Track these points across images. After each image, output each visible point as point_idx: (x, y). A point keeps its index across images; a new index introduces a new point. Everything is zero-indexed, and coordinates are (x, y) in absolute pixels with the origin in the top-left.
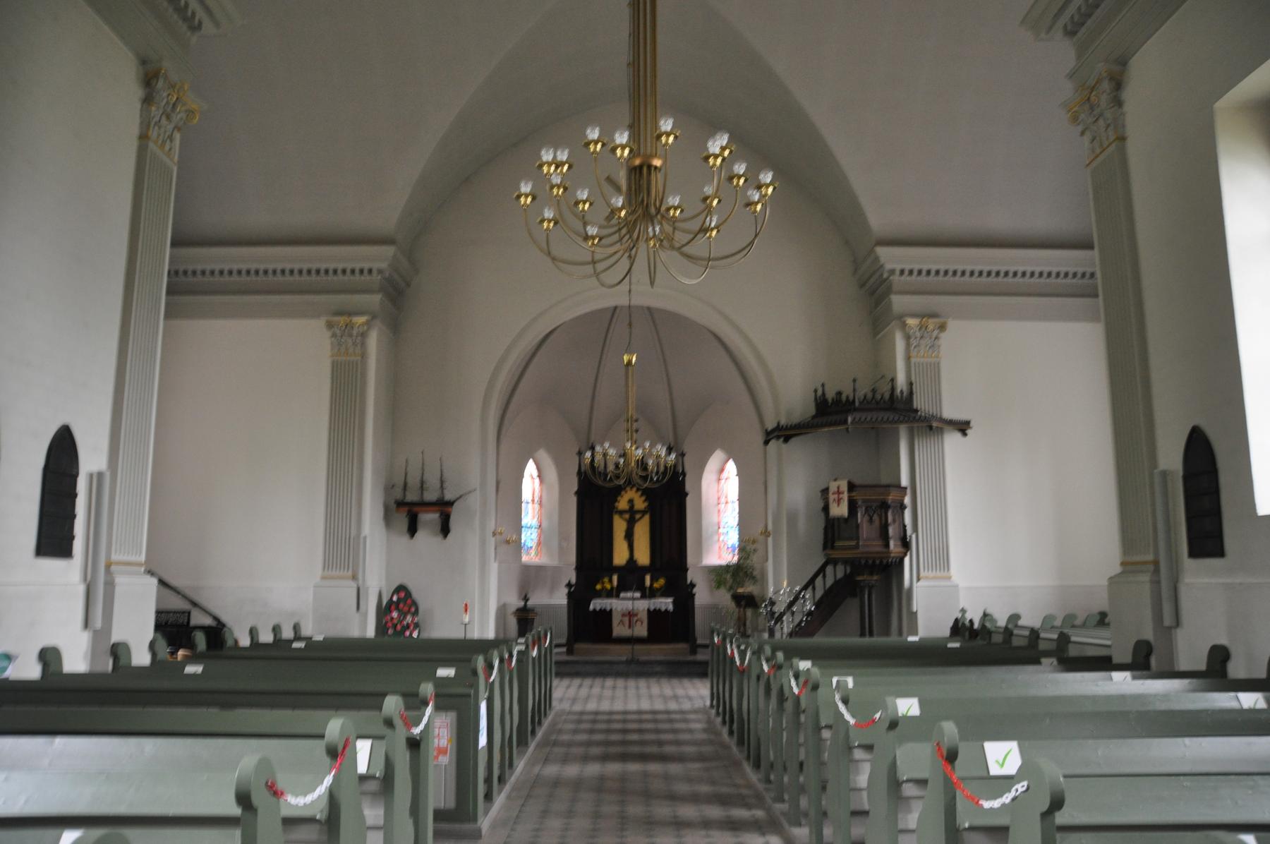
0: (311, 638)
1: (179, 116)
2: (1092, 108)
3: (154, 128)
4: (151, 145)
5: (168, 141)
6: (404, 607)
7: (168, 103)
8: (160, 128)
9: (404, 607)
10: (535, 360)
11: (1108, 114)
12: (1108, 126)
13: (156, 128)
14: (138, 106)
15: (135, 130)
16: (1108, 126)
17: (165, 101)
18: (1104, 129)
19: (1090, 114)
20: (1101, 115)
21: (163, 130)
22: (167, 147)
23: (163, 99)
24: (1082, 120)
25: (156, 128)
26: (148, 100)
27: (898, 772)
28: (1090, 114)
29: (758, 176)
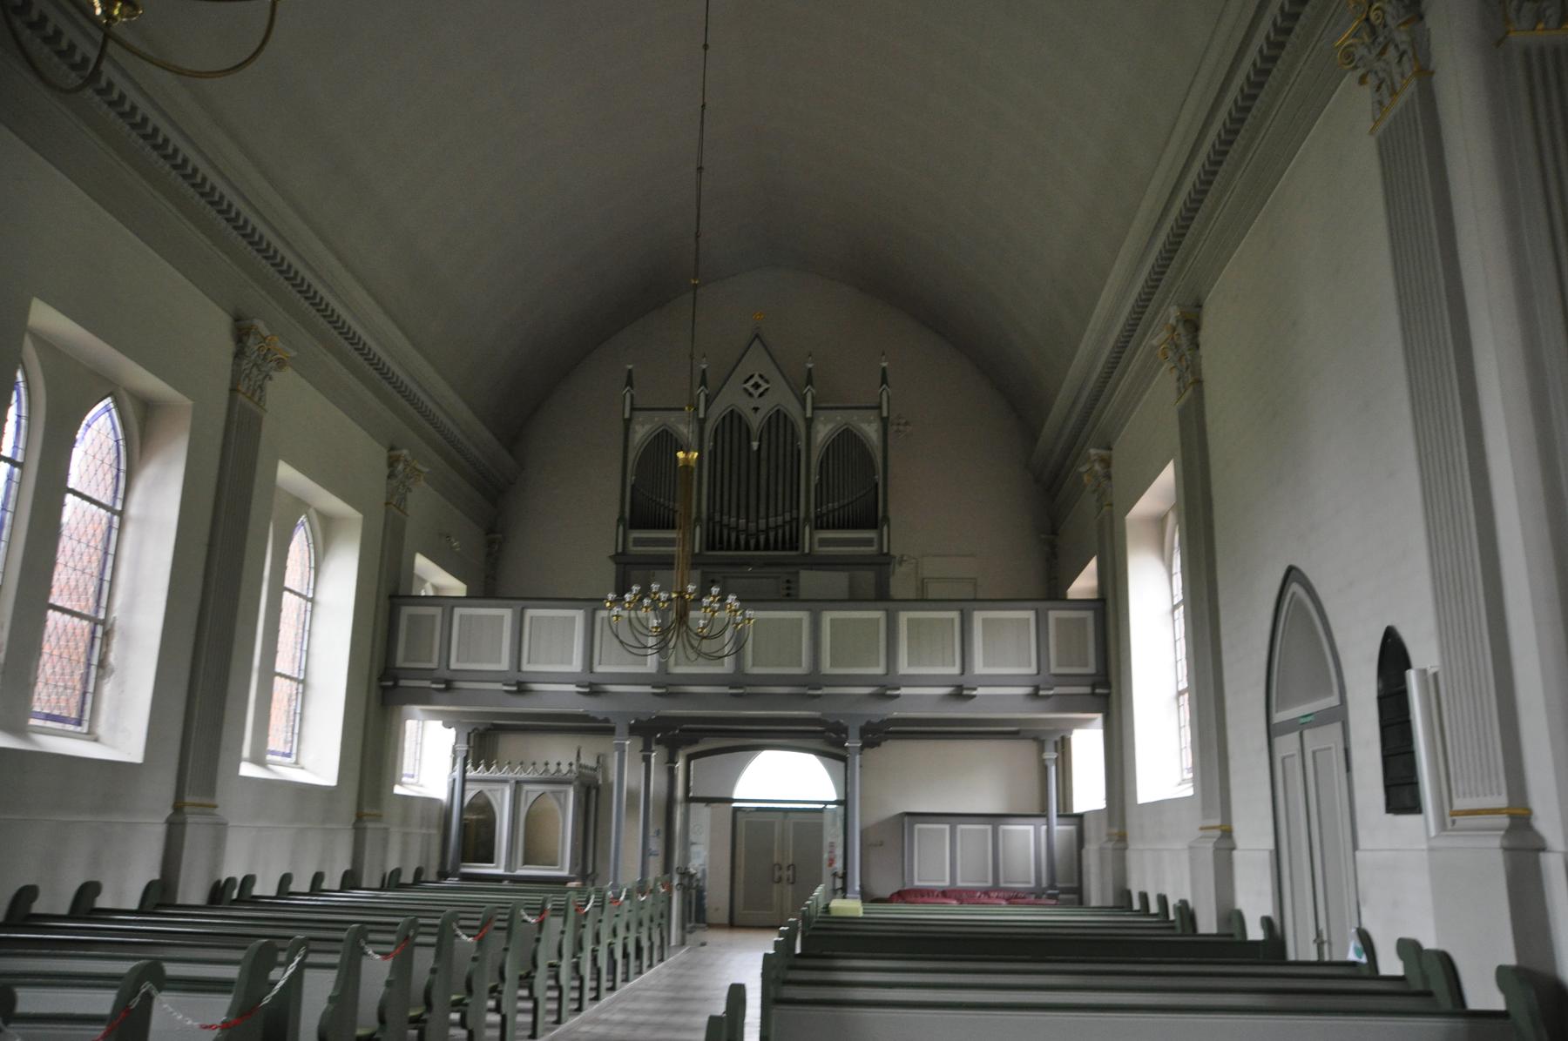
0: (1543, 849)
1: (270, 365)
2: (1373, 32)
3: (244, 380)
4: (241, 397)
5: (259, 391)
6: (629, 615)
7: (258, 356)
8: (250, 380)
9: (629, 615)
10: (567, 596)
11: (1402, 37)
12: (1402, 56)
13: (247, 380)
14: (230, 360)
15: (226, 384)
16: (1402, 56)
17: (256, 354)
18: (1396, 60)
19: (1373, 42)
20: (1389, 41)
21: (252, 383)
22: (256, 399)
23: (254, 352)
24: (1361, 58)
25: (247, 380)
26: (239, 354)
27: (352, 839)
28: (1373, 42)
29: (624, 594)
